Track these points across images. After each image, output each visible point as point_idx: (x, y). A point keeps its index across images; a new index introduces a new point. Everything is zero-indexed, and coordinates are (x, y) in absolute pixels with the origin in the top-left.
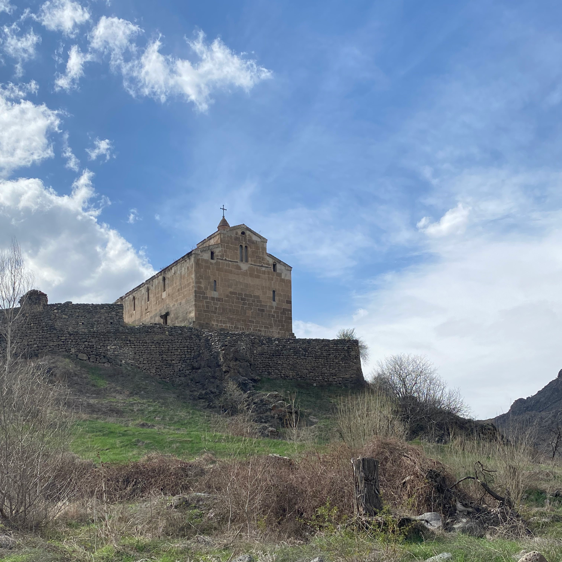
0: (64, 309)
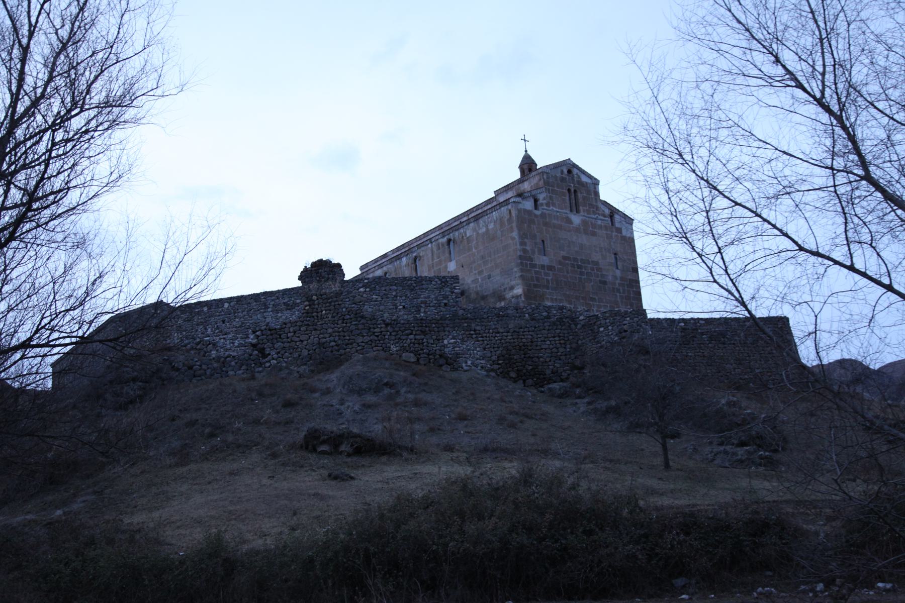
0: (373, 286)
